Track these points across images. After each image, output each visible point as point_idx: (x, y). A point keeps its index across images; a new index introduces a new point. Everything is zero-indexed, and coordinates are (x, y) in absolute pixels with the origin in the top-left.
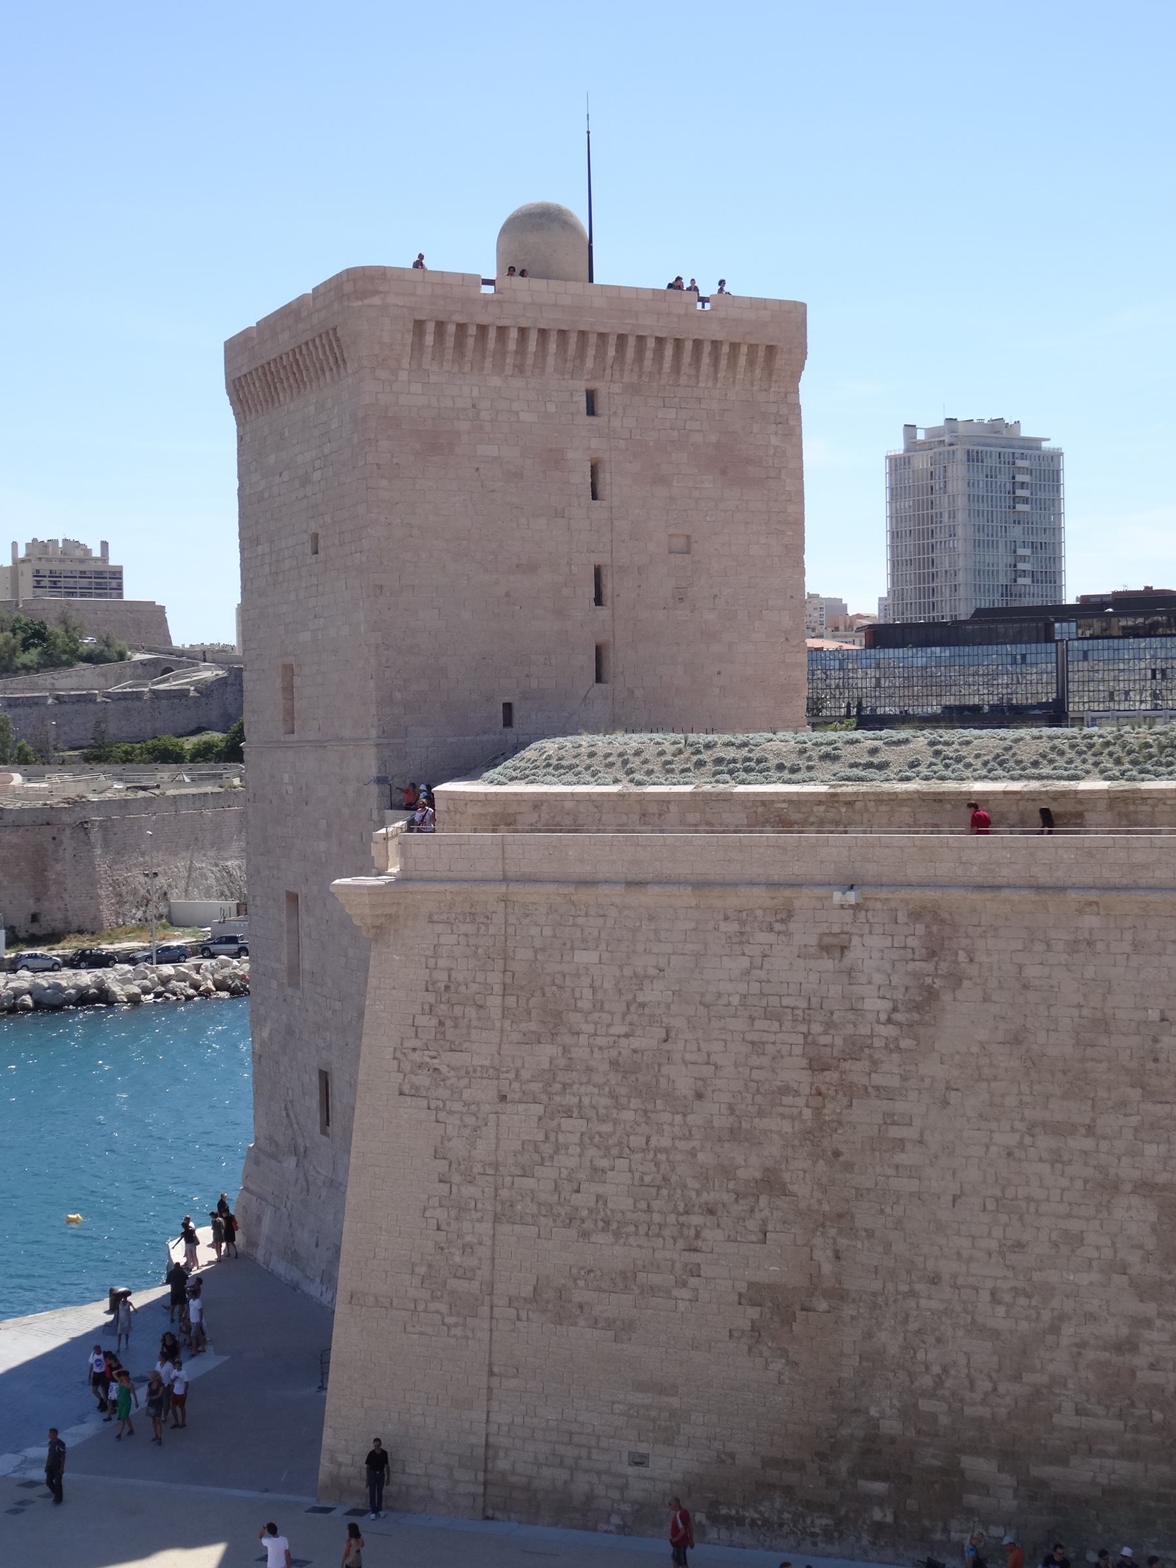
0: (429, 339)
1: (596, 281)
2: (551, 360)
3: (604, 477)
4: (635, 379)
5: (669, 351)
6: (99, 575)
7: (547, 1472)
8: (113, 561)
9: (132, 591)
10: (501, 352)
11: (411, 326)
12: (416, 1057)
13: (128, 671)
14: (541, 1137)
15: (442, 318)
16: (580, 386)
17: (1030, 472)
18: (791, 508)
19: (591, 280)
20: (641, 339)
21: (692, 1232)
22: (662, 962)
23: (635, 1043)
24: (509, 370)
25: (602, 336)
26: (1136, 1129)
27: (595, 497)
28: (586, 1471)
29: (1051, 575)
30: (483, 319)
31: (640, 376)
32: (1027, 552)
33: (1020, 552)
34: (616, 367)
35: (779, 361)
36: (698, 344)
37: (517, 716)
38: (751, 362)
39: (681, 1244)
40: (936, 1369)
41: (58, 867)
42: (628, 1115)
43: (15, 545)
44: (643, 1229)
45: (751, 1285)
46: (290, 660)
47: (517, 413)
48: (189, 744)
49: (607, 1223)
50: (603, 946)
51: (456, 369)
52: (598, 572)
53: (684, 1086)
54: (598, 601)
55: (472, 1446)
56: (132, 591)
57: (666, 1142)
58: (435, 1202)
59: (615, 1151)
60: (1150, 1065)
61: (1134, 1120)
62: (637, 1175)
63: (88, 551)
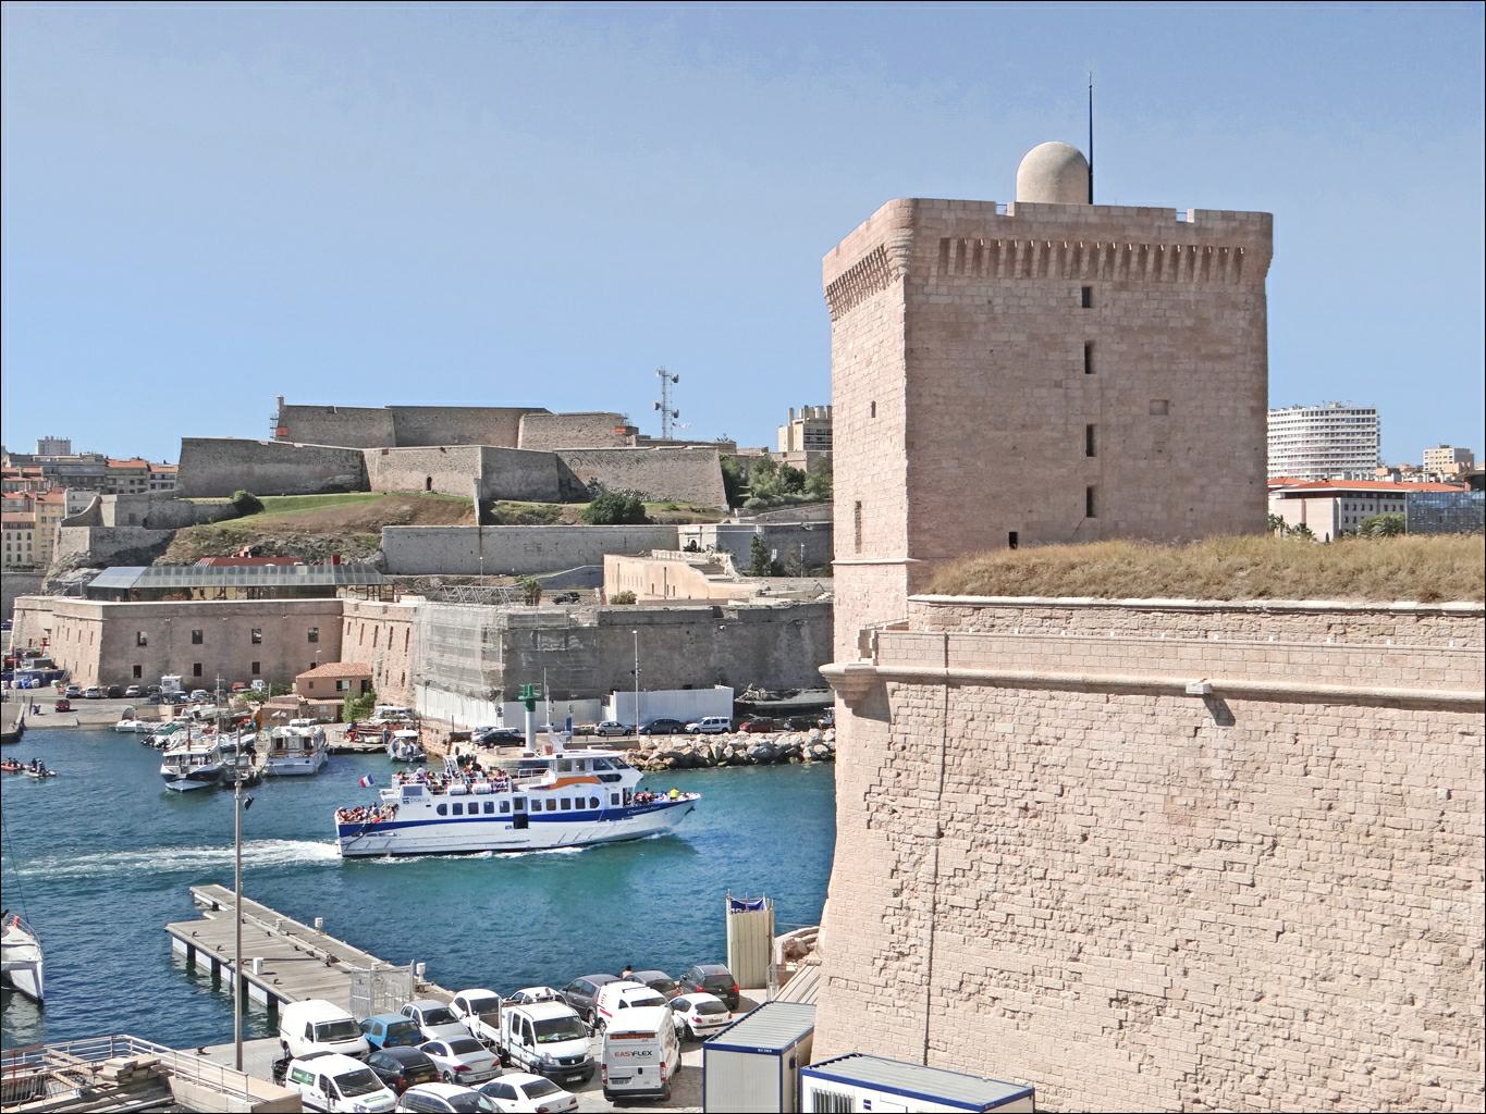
0: (953, 253)
1: (1096, 202)
3: (1097, 356)
4: (1123, 279)
5: (1151, 257)
10: (1012, 261)
12: (880, 799)
22: (1060, 733)
23: (1038, 796)
27: (1088, 370)
31: (1127, 275)
34: (1107, 269)
39: (1068, 955)
41: (776, 654)
42: (1031, 853)
47: (1024, 307)
52: (1090, 430)
53: (1073, 828)
54: (1090, 452)
58: (890, 911)
59: (1020, 879)
60: (1438, 835)
61: (1423, 879)
62: (1037, 899)
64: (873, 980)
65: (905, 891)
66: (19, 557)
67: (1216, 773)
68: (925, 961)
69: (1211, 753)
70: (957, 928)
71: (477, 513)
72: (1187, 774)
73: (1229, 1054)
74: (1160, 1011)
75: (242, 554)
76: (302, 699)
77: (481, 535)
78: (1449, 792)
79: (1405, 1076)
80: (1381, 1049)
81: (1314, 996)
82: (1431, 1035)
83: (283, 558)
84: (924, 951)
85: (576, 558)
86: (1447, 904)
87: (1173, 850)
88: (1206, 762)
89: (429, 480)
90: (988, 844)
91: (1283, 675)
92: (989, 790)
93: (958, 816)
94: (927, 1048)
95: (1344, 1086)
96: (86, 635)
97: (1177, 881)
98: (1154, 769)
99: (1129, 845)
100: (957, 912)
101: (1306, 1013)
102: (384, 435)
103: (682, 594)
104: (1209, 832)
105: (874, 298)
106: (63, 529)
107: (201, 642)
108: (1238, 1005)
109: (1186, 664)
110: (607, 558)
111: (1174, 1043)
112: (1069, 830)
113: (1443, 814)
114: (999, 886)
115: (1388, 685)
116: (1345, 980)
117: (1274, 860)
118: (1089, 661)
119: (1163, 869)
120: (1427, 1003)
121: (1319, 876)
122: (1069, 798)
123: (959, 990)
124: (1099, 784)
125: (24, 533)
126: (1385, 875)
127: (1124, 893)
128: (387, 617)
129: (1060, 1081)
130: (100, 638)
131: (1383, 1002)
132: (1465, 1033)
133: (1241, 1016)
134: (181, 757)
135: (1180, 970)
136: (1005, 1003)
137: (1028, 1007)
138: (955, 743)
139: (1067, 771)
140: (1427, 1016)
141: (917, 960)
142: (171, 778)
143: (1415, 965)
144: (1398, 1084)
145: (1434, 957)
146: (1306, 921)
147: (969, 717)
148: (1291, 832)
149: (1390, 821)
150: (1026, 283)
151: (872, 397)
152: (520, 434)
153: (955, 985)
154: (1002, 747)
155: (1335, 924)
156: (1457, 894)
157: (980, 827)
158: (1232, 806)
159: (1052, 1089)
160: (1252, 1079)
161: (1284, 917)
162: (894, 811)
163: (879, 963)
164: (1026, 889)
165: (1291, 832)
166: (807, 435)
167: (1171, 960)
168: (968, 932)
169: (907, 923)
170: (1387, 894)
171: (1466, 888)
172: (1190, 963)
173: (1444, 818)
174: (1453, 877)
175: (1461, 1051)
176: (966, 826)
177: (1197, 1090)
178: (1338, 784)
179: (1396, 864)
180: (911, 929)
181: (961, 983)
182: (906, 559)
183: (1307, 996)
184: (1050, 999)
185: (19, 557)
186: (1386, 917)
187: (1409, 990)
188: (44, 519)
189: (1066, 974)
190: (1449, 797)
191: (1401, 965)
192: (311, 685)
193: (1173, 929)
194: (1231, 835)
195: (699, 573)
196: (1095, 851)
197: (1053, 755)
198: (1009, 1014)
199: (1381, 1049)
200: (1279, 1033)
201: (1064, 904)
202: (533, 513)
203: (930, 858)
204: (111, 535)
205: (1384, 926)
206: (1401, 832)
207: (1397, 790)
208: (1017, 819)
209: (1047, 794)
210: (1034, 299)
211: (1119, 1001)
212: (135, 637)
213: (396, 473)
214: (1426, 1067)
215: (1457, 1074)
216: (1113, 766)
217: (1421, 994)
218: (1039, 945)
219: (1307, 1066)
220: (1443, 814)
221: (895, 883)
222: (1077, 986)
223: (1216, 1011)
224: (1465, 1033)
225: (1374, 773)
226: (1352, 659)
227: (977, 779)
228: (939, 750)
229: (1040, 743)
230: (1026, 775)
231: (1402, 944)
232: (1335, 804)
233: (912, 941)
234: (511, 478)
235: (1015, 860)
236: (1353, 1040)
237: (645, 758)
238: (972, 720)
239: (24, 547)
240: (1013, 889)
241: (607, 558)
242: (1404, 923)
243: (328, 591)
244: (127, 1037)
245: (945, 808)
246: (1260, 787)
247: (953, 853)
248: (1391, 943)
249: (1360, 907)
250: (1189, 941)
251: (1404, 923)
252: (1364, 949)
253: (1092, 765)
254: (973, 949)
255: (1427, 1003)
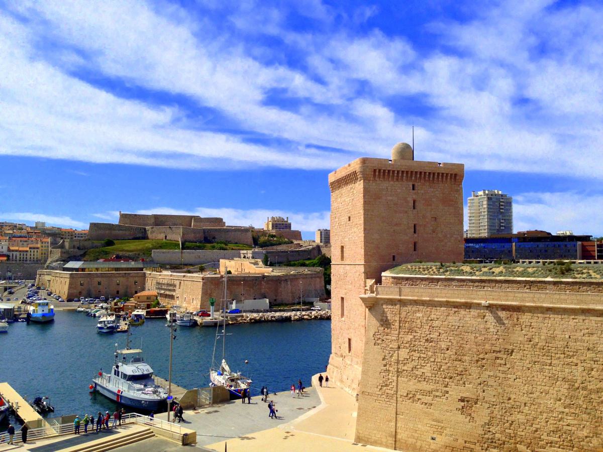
0: (377, 173)
1: (415, 160)
2: (404, 178)
3: (417, 204)
5: (432, 176)
6: (286, 224)
7: (410, 440)
8: (289, 222)
9: (293, 228)
10: (398, 176)
11: (373, 170)
12: (378, 336)
13: (293, 246)
14: (408, 357)
15: (380, 168)
16: (411, 184)
17: (503, 202)
18: (460, 211)
19: (413, 160)
20: (425, 173)
21: (446, 383)
22: (438, 317)
24: (395, 180)
25: (416, 172)
26: (563, 365)
27: (414, 209)
28: (420, 440)
29: (509, 227)
30: (398, 169)
32: (503, 221)
33: (501, 221)
35: (457, 178)
36: (438, 174)
37: (396, 259)
38: (451, 178)
39: (443, 385)
40: (510, 422)
41: (281, 289)
42: (430, 354)
43: (268, 218)
44: (434, 381)
45: (461, 397)
46: (342, 245)
48: (307, 262)
49: (425, 378)
50: (423, 313)
51: (383, 180)
52: (415, 226)
53: (444, 346)
54: (415, 232)
55: (392, 432)
56: (293, 228)
57: (439, 360)
59: (426, 362)
60: (566, 349)
61: (562, 363)
62: (432, 368)
63: (283, 219)
64: (377, 393)
65: (388, 365)
66: (23, 257)
67: (492, 330)
68: (395, 387)
69: (490, 323)
70: (406, 377)
71: (181, 247)
72: (482, 330)
73: (499, 417)
74: (476, 403)
75: (113, 258)
76: (136, 302)
77: (182, 253)
78: (570, 336)
79: (558, 423)
80: (550, 415)
81: (527, 399)
82: (567, 410)
83: (127, 259)
84: (394, 384)
85: (210, 260)
86: (570, 370)
87: (478, 353)
88: (488, 326)
89: (166, 237)
90: (415, 351)
91: (513, 300)
92: (415, 334)
93: (405, 342)
94: (397, 414)
95: (539, 426)
96: (63, 282)
97: (480, 363)
98: (471, 328)
99: (463, 351)
100: (405, 372)
101: (525, 404)
102: (152, 222)
103: (247, 271)
104: (490, 348)
105: (350, 186)
106: (52, 250)
107: (100, 284)
108: (502, 401)
109: (480, 297)
110: (221, 260)
111: (482, 414)
112: (442, 347)
113: (568, 343)
114: (419, 364)
115: (549, 304)
116: (538, 394)
117: (512, 357)
118: (472, 296)
119: (476, 358)
120: (565, 401)
121: (527, 361)
122: (442, 336)
123: (407, 396)
124: (452, 333)
125: (36, 250)
126: (549, 361)
127: (462, 366)
128: (151, 276)
129: (442, 425)
130: (68, 284)
131: (550, 400)
132: (578, 409)
133: (503, 405)
134: (104, 321)
135: (482, 390)
136: (423, 400)
137: (430, 402)
138: (403, 319)
139: (441, 328)
140: (565, 405)
141: (392, 386)
142: (101, 328)
143: (560, 389)
144: (556, 426)
145: (567, 386)
146: (524, 375)
147: (408, 312)
148: (517, 348)
149: (550, 345)
150: (397, 183)
151: (349, 215)
152: (192, 223)
153: (405, 394)
154: (419, 321)
155: (534, 377)
156: (573, 367)
157: (412, 345)
158: (497, 340)
159: (440, 427)
160: (507, 425)
161: (517, 374)
162: (383, 340)
163: (380, 387)
164: (429, 365)
165: (517, 348)
166: (273, 225)
167: (479, 387)
168: (409, 378)
169: (388, 375)
170: (551, 367)
171: (576, 365)
172: (485, 388)
173: (568, 344)
174: (572, 362)
175: (577, 415)
176: (407, 345)
177: (489, 428)
178: (533, 333)
179: (553, 358)
180: (390, 377)
181: (408, 394)
182: (363, 263)
183: (525, 399)
184: (438, 399)
185: (23, 257)
186: (550, 374)
187: (559, 397)
188: (42, 246)
189: (443, 391)
190: (570, 338)
191: (556, 389)
192: (139, 298)
193: (479, 378)
194: (498, 349)
195: (253, 265)
196: (452, 353)
197: (436, 324)
198: (424, 404)
199: (550, 415)
200: (516, 410)
201: (441, 370)
202: (197, 246)
203: (396, 354)
204: (67, 252)
205: (550, 377)
206: (554, 349)
207: (552, 336)
208: (424, 343)
209: (434, 335)
210: (399, 187)
211: (462, 400)
212: (80, 283)
213: (157, 235)
214: (565, 420)
215: (576, 422)
216: (457, 327)
217: (563, 398)
218: (434, 382)
219: (526, 420)
220: (568, 343)
221: (384, 362)
222: (447, 395)
223: (495, 403)
224: (578, 409)
225: (544, 331)
226: (536, 295)
227: (411, 331)
228: (398, 322)
229: (432, 320)
230: (427, 330)
231: (556, 382)
232: (532, 340)
233: (390, 381)
234: (191, 236)
235: (425, 356)
236: (541, 412)
237: (245, 320)
238: (409, 313)
239: (32, 255)
240: (424, 364)
241: (221, 260)
242: (556, 376)
243: (141, 269)
244: (135, 414)
245: (400, 339)
246: (507, 334)
247: (404, 353)
248: (552, 382)
249: (541, 371)
250: (484, 382)
251: (556, 376)
252: (543, 384)
253: (449, 327)
254: (411, 383)
255: (565, 401)
